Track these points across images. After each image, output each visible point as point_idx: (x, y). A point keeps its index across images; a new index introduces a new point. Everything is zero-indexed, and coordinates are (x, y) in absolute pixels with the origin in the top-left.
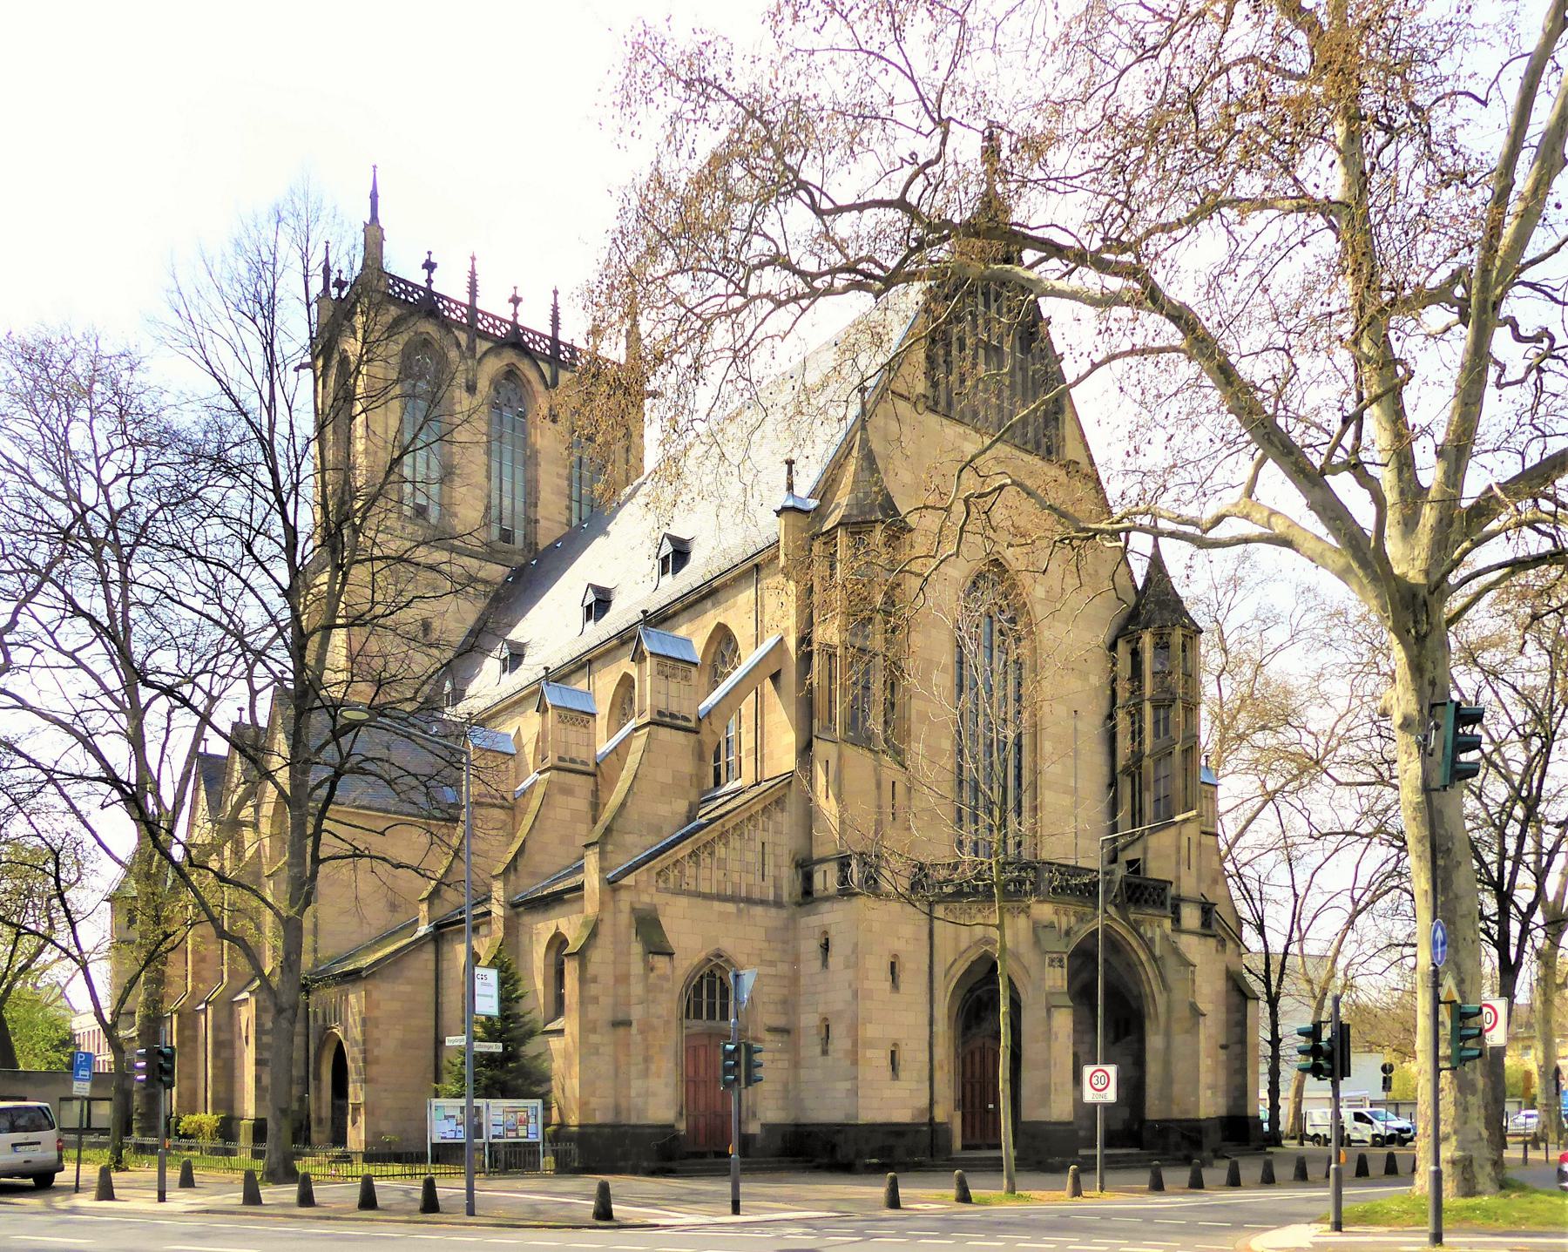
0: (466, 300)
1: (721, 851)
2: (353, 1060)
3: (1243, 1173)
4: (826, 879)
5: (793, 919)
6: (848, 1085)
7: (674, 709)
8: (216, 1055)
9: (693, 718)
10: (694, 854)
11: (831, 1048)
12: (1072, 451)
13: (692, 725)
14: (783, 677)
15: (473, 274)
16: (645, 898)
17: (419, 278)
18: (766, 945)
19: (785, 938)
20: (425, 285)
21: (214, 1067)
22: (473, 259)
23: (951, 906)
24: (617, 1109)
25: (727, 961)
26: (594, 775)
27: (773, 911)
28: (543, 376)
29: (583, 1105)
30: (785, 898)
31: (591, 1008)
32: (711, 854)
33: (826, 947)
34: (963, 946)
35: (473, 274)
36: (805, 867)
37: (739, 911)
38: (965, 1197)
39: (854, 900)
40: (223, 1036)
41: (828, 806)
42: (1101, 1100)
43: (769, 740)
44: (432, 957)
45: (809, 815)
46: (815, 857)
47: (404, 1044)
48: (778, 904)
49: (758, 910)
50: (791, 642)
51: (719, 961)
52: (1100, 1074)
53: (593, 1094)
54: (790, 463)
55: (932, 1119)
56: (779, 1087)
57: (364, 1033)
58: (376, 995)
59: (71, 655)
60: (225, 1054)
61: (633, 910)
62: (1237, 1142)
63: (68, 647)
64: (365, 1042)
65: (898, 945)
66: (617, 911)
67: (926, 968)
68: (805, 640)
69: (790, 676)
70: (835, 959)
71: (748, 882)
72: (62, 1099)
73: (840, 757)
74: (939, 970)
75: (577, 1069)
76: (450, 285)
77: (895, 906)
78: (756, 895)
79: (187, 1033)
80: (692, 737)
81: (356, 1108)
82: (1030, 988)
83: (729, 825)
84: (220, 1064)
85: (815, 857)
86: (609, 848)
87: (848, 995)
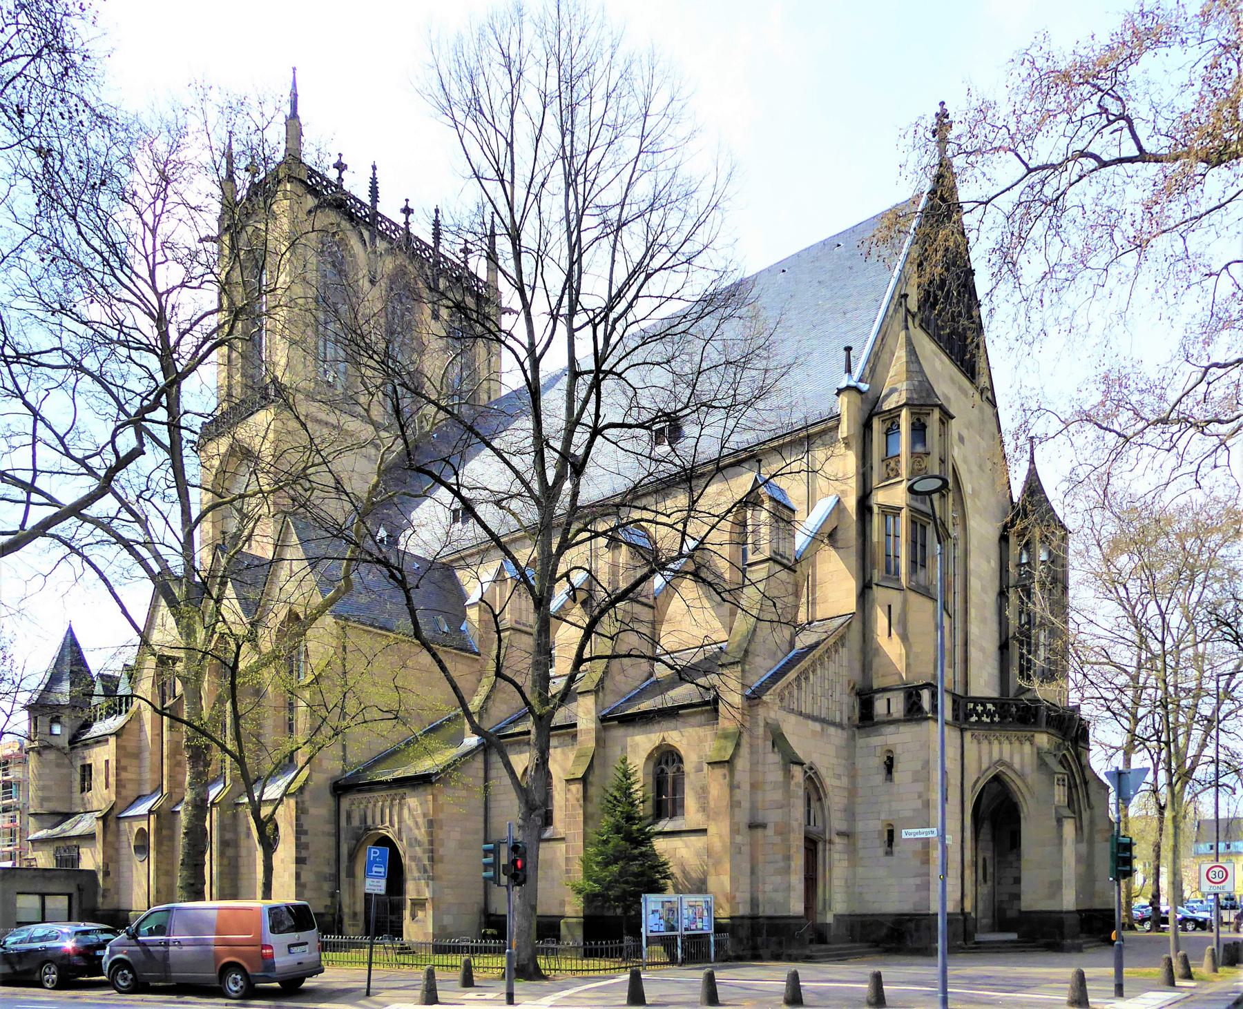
2: (413, 858)
3: (477, 975)
4: (890, 705)
5: (853, 738)
6: (918, 881)
8: (222, 854)
10: (798, 678)
11: (895, 849)
12: (983, 381)
14: (840, 535)
15: (374, 181)
16: (772, 715)
19: (850, 754)
21: (221, 865)
22: (374, 168)
23: (976, 733)
24: (754, 903)
26: (651, 607)
27: (840, 731)
29: (731, 899)
31: (737, 810)
33: (889, 765)
34: (984, 766)
35: (374, 181)
36: (865, 698)
39: (925, 724)
40: (228, 836)
41: (891, 648)
43: (835, 587)
44: (482, 765)
45: (868, 650)
46: (875, 687)
47: (462, 845)
50: (851, 503)
53: (737, 890)
54: (848, 349)
55: (962, 909)
56: (843, 883)
57: (430, 834)
58: (441, 799)
59: (82, 462)
60: (230, 852)
61: (767, 724)
62: (1096, 927)
63: (79, 454)
64: (431, 843)
66: (756, 724)
68: (864, 506)
69: (850, 532)
70: (902, 772)
71: (822, 707)
73: (905, 602)
74: (968, 785)
75: (728, 866)
79: (165, 832)
81: (419, 904)
82: (1030, 801)
84: (225, 862)
85: (875, 687)
87: (918, 804)
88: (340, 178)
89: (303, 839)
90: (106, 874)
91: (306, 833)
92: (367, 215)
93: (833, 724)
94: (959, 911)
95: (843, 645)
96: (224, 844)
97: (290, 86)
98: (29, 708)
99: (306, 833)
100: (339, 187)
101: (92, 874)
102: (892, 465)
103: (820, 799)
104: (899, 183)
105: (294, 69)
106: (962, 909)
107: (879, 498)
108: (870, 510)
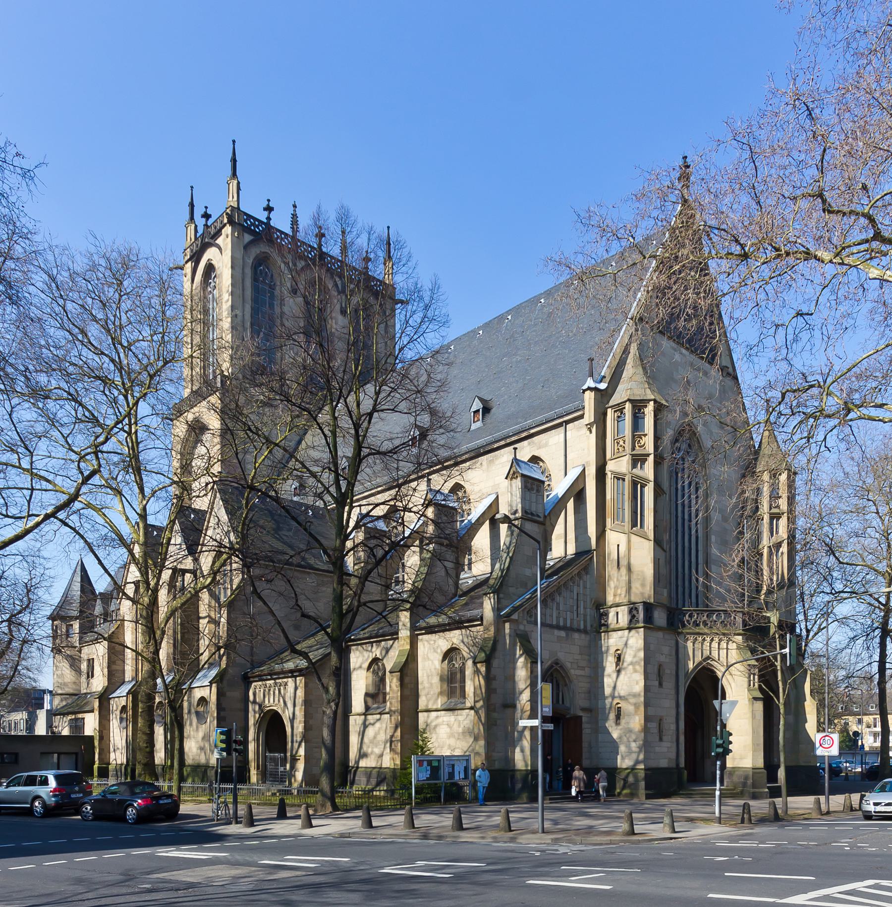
0: (288, 231)
1: (558, 598)
7: (533, 509)
9: (541, 515)
13: (541, 520)
16: (522, 627)
17: (262, 216)
18: (579, 657)
20: (265, 221)
22: (295, 206)
25: (561, 667)
27: (583, 636)
28: (336, 285)
30: (589, 628)
32: (553, 600)
37: (567, 635)
38: (370, 825)
42: (826, 754)
48: (585, 631)
49: (576, 635)
51: (556, 667)
52: (827, 738)
54: (591, 360)
65: (662, 659)
67: (674, 673)
72: (42, 753)
73: (629, 541)
76: (281, 222)
77: (660, 634)
78: (575, 626)
80: (542, 527)
83: (562, 583)
86: (501, 596)
88: (269, 218)
89: (222, 714)
90: (101, 738)
91: (224, 709)
92: (290, 243)
93: (578, 630)
94: (674, 766)
95: (587, 573)
96: (751, 834)
97: (231, 155)
98: (52, 618)
99: (224, 709)
100: (268, 224)
101: (91, 738)
102: (621, 443)
103: (566, 685)
104: (650, 224)
105: (234, 142)
106: (678, 765)
107: (611, 466)
108: (605, 475)
